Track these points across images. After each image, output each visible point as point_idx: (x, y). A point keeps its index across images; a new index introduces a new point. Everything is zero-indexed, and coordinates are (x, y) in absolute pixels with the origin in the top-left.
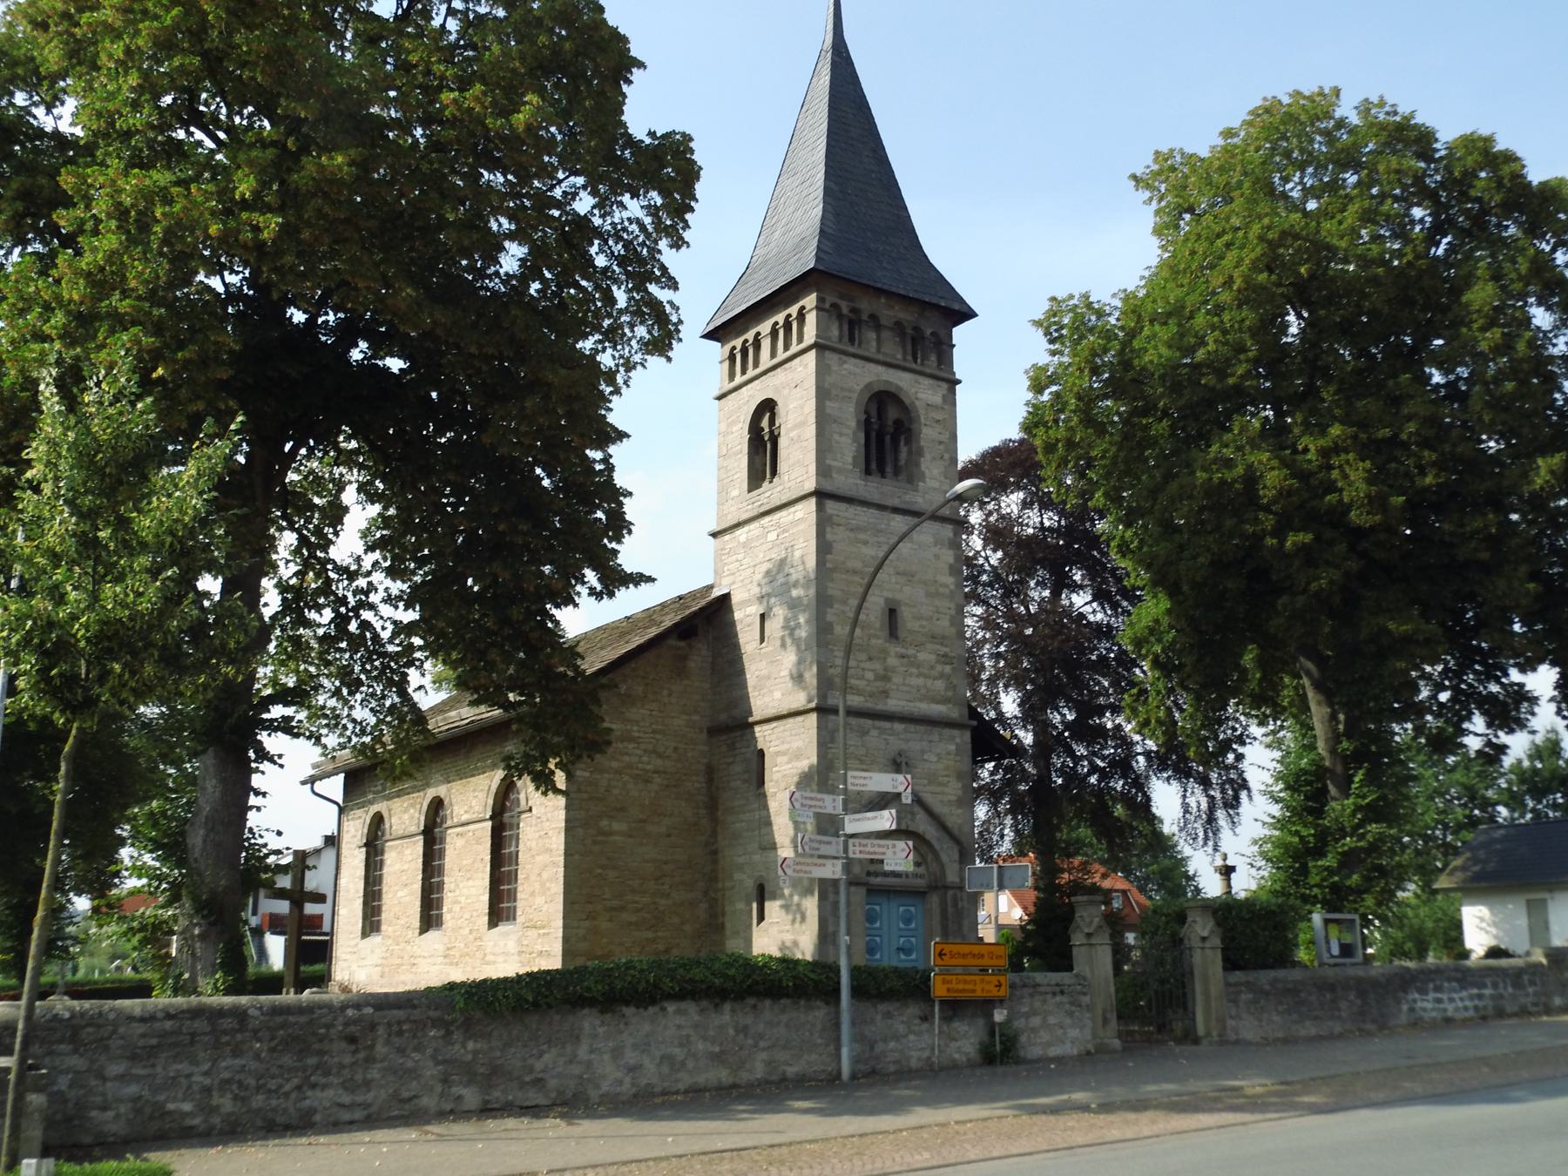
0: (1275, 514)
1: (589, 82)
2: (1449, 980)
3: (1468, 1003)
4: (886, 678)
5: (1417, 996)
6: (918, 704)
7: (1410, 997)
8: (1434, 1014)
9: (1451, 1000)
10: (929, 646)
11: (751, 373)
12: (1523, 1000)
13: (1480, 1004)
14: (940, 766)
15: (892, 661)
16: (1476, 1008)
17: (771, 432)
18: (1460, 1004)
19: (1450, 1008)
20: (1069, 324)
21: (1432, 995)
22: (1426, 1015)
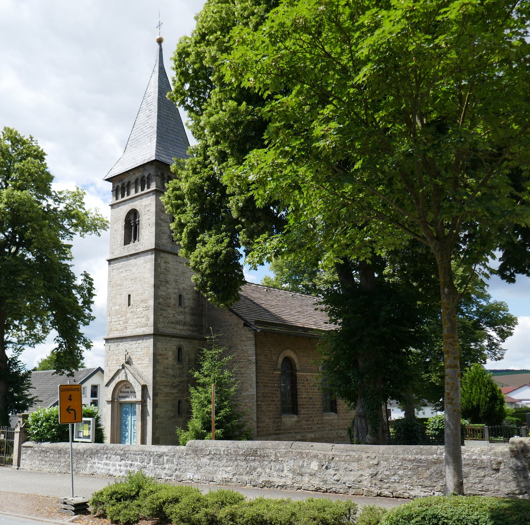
0: (309, 105)
1: (421, 43)
2: (116, 454)
3: (122, 468)
4: (127, 322)
5: (96, 460)
6: (138, 329)
7: (93, 461)
8: (103, 471)
9: (114, 465)
10: (141, 305)
11: (126, 198)
12: (158, 471)
13: (131, 469)
14: (142, 353)
15: (129, 315)
16: (126, 471)
17: (135, 223)
18: (118, 468)
19: (112, 469)
20: (489, 2)
21: (105, 461)
22: (99, 471)
